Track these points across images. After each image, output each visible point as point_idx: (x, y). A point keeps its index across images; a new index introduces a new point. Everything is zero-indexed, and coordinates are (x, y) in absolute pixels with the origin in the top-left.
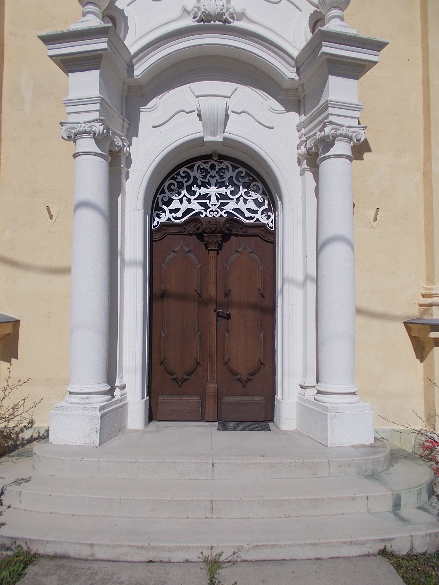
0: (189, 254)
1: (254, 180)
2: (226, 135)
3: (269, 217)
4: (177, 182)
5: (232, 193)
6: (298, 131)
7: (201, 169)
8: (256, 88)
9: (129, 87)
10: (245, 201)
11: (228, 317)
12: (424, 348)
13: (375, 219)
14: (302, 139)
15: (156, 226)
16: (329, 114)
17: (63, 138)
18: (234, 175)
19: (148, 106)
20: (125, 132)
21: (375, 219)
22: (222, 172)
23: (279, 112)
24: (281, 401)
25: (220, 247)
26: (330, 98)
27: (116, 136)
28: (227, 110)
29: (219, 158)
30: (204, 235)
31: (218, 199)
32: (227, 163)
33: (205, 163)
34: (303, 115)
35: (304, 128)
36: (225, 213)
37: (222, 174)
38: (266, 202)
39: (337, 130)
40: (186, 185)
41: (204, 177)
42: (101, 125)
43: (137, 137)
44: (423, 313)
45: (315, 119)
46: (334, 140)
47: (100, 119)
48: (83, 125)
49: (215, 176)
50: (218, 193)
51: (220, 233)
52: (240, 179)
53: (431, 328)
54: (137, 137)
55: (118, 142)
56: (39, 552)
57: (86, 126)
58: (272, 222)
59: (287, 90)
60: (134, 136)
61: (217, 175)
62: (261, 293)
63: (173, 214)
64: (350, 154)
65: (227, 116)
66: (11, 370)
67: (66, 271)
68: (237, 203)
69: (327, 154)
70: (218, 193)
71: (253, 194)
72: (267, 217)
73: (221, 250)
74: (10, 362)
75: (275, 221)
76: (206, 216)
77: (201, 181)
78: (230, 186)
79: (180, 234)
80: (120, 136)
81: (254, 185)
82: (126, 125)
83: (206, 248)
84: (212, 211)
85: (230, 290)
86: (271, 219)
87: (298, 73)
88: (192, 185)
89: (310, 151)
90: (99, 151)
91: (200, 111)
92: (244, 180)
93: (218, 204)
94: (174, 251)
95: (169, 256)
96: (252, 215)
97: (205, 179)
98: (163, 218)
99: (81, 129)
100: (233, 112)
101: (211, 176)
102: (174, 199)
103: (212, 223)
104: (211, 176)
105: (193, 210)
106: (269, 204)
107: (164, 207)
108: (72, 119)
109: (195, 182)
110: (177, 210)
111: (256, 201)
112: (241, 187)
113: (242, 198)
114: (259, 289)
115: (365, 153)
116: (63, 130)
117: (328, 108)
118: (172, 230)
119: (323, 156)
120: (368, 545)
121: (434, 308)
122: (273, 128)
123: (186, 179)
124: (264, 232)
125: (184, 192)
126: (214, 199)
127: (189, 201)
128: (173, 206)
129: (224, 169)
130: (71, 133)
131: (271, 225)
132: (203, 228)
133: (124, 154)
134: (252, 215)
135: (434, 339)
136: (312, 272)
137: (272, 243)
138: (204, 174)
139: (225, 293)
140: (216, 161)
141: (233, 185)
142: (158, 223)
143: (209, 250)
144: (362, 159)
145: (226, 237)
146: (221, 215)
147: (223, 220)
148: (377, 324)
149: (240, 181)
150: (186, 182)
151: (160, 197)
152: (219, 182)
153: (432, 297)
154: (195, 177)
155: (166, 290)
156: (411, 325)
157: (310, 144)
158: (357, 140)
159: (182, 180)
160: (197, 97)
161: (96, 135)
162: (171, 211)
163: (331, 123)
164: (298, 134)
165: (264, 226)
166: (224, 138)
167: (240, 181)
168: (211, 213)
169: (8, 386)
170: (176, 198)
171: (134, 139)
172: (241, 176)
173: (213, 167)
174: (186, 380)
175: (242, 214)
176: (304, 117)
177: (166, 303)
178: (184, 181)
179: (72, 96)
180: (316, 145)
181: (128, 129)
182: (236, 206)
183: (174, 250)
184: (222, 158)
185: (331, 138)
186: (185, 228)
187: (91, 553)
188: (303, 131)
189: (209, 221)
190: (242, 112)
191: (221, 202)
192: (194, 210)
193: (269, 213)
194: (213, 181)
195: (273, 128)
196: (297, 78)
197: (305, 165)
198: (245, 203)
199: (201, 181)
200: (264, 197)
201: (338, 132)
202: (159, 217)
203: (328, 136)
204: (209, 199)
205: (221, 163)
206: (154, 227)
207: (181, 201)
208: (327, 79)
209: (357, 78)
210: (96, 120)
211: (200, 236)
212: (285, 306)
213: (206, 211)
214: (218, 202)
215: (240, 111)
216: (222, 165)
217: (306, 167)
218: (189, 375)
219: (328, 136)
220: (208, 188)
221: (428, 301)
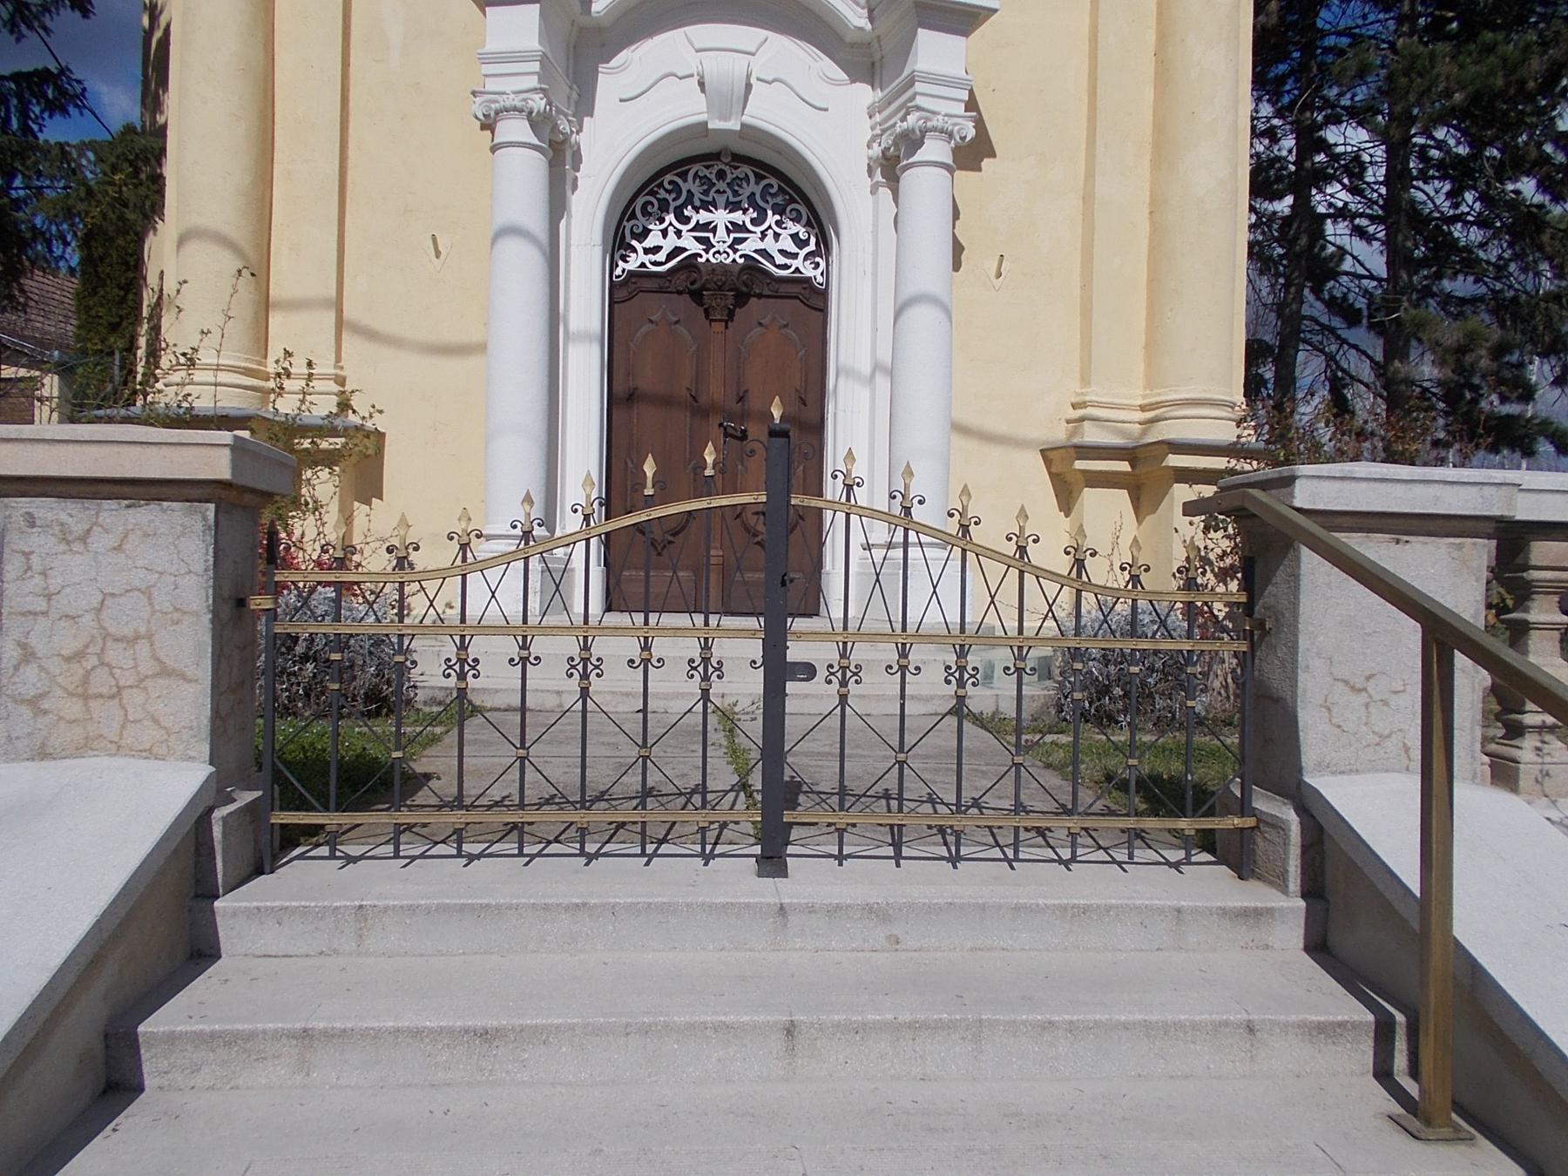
0: (677, 326)
1: (792, 200)
2: (746, 119)
3: (817, 265)
4: (658, 199)
5: (753, 221)
6: (870, 117)
7: (700, 178)
8: (800, 39)
9: (581, 29)
10: (777, 236)
11: (744, 436)
12: (1071, 493)
13: (999, 275)
14: (875, 132)
15: (619, 276)
16: (916, 94)
17: (476, 118)
18: (758, 190)
19: (612, 63)
20: (572, 108)
21: (999, 275)
22: (738, 185)
23: (839, 83)
24: (832, 571)
25: (731, 314)
26: (917, 68)
27: (561, 117)
28: (748, 76)
29: (733, 160)
30: (705, 293)
31: (729, 231)
32: (746, 169)
33: (707, 167)
34: (879, 90)
35: (879, 112)
36: (741, 257)
37: (736, 188)
38: (813, 240)
39: (927, 119)
40: (673, 205)
41: (706, 193)
42: (541, 99)
43: (592, 116)
44: (1072, 435)
45: (897, 98)
46: (923, 137)
47: (541, 89)
48: (512, 96)
49: (724, 192)
50: (730, 222)
51: (731, 290)
52: (769, 199)
53: (1076, 453)
54: (592, 116)
55: (564, 126)
56: (484, 704)
57: (516, 99)
58: (822, 274)
59: (853, 45)
60: (587, 116)
61: (727, 190)
62: (801, 398)
63: (651, 257)
64: (949, 160)
65: (749, 87)
66: (371, 517)
67: (480, 348)
68: (762, 239)
69: (911, 160)
70: (730, 222)
71: (790, 224)
72: (813, 266)
73: (732, 321)
74: (369, 503)
75: (827, 274)
76: (708, 260)
77: (701, 200)
78: (751, 210)
79: (660, 291)
80: (566, 115)
81: (791, 210)
82: (575, 96)
83: (707, 317)
84: (718, 252)
85: (746, 391)
86: (820, 270)
87: (871, 19)
88: (684, 205)
89: (887, 153)
90: (535, 141)
91: (702, 77)
92: (775, 201)
93: (730, 241)
94: (651, 321)
95: (642, 330)
96: (788, 261)
97: (708, 196)
98: (633, 263)
99: (508, 104)
100: (758, 79)
101: (718, 192)
102: (651, 230)
103: (717, 272)
104: (718, 192)
105: (685, 250)
106: (817, 244)
107: (634, 243)
108: (492, 85)
109: (689, 200)
110: (657, 249)
111: (795, 237)
112: (770, 213)
113: (770, 231)
114: (797, 390)
115: (985, 160)
116: (477, 105)
117: (913, 84)
118: (648, 284)
119: (905, 162)
120: (934, 701)
121: (1086, 423)
122: (826, 110)
123: (673, 195)
124: (808, 291)
125: (670, 218)
126: (721, 231)
127: (679, 233)
128: (650, 242)
129: (741, 179)
130: (491, 108)
131: (820, 279)
132: (703, 281)
133: (571, 147)
134: (788, 261)
135: (1084, 472)
136: (885, 357)
137: (821, 310)
138: (705, 187)
139: (738, 394)
140: (726, 164)
141: (757, 207)
142: (623, 271)
143: (711, 321)
144: (979, 169)
145: (742, 298)
146: (734, 260)
147: (737, 269)
148: (995, 452)
149: (767, 202)
150: (674, 200)
151: (628, 225)
152: (732, 203)
153: (1086, 407)
154: (689, 191)
155: (636, 389)
156: (1050, 454)
157: (887, 140)
158: (961, 138)
159: (667, 196)
160: (697, 51)
161: (534, 114)
162: (647, 251)
163: (918, 108)
164: (869, 123)
165: (808, 280)
166: (743, 125)
167: (767, 202)
168: (717, 255)
169: (716, 390)
170: (655, 227)
171: (586, 120)
172: (770, 194)
173: (721, 175)
174: (670, 542)
175: (770, 258)
176: (879, 94)
177: (636, 411)
178: (670, 198)
179: (492, 46)
180: (895, 143)
181: (576, 103)
182: (761, 246)
183: (652, 318)
184: (739, 159)
185: (918, 132)
186: (670, 281)
187: (558, 702)
188: (878, 118)
189: (713, 270)
190: (774, 80)
191: (735, 238)
192: (685, 250)
193: (818, 259)
194: (721, 200)
195: (826, 110)
196: (869, 27)
197: (878, 177)
198: (777, 241)
199: (701, 200)
200: (810, 229)
201: (929, 124)
202: (624, 259)
203: (913, 130)
204: (714, 230)
205: (736, 168)
206: (617, 277)
207: (665, 233)
208: (915, 34)
209: (965, 33)
210: (534, 90)
211: (697, 296)
212: (840, 414)
213: (707, 253)
214: (729, 236)
215: (770, 79)
216: (737, 173)
217: (881, 179)
218: (674, 535)
219: (913, 130)
220: (711, 211)
221: (1080, 413)
